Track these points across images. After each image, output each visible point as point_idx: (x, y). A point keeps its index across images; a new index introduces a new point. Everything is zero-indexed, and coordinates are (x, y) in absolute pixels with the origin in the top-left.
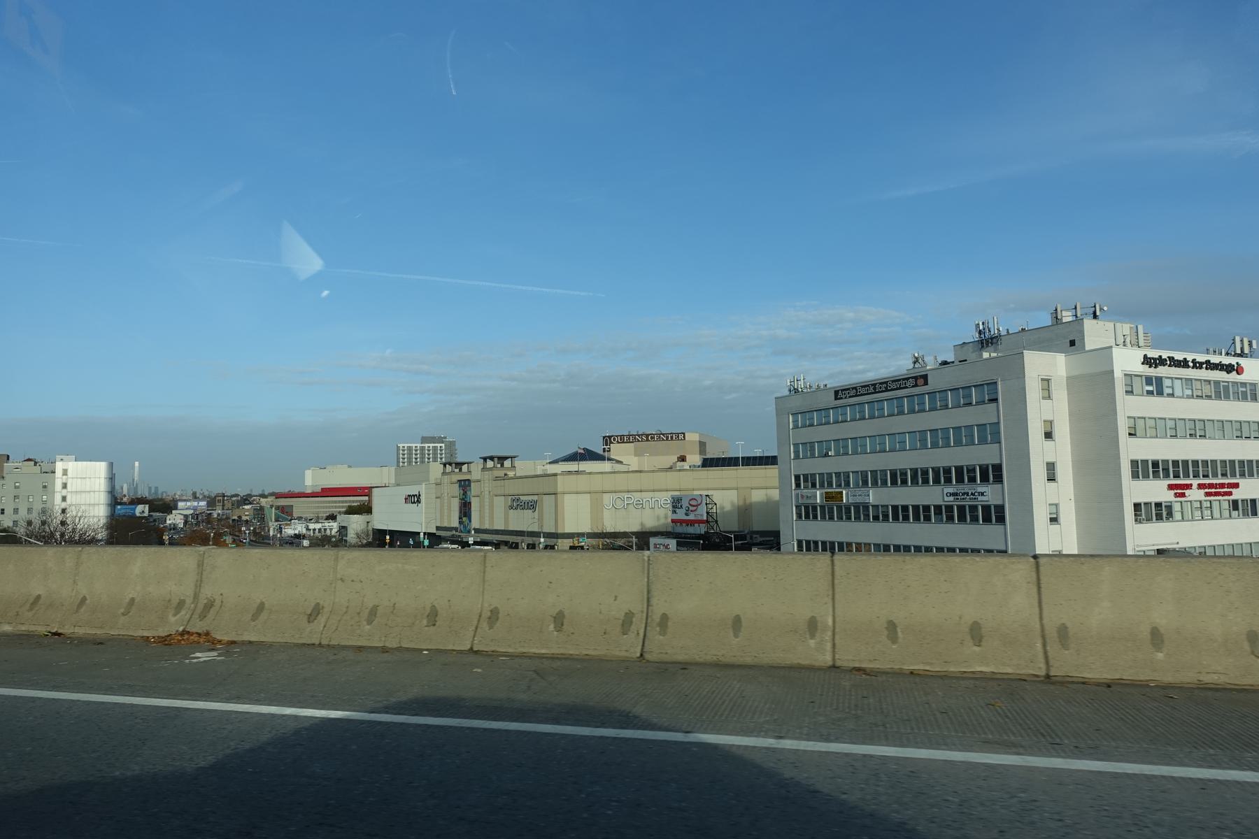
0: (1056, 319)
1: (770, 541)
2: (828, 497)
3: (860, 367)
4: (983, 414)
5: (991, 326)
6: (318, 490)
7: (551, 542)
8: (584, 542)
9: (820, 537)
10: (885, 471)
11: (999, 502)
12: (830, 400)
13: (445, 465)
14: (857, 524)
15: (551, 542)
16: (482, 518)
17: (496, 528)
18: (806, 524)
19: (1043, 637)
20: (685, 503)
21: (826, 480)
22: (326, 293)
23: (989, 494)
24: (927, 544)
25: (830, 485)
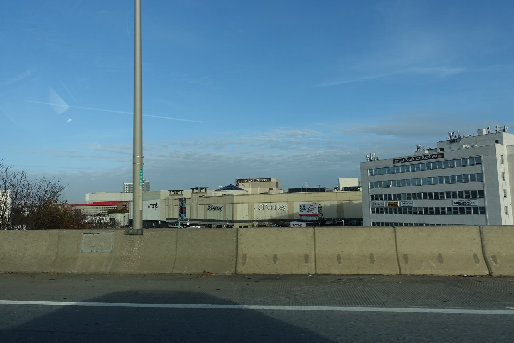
0: (480, 131)
1: (358, 222)
2: (390, 204)
3: (305, 153)
4: (475, 170)
5: (457, 135)
6: (92, 202)
7: (231, 224)
8: (266, 224)
9: (385, 221)
10: (382, 195)
11: (482, 206)
12: (391, 164)
13: (170, 191)
14: (406, 215)
15: (231, 224)
16: (191, 214)
17: (199, 218)
18: (376, 215)
19: (398, 259)
20: (307, 207)
21: (388, 197)
22: (70, 120)
23: (477, 202)
24: (401, 222)
25: (390, 199)
